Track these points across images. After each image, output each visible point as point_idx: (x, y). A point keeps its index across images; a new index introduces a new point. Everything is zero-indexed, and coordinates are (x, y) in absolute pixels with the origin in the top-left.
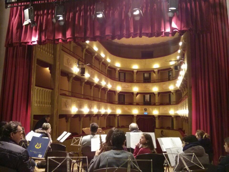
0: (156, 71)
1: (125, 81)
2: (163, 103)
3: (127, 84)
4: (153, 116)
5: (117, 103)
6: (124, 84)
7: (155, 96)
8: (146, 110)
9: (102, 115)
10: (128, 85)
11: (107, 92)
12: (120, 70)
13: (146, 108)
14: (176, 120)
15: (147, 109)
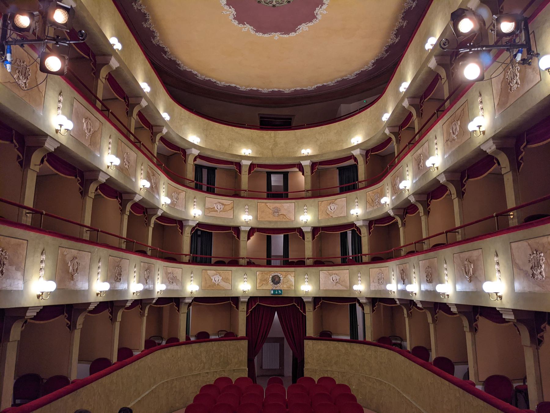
0: (306, 166)
1: (211, 191)
2: (323, 260)
3: (220, 201)
4: (299, 300)
5: (186, 259)
6: (212, 200)
7: (304, 238)
8: (277, 279)
9: (129, 304)
10: (223, 204)
11: (153, 220)
12: (200, 157)
13: (276, 274)
14: (373, 311)
15: (281, 279)
